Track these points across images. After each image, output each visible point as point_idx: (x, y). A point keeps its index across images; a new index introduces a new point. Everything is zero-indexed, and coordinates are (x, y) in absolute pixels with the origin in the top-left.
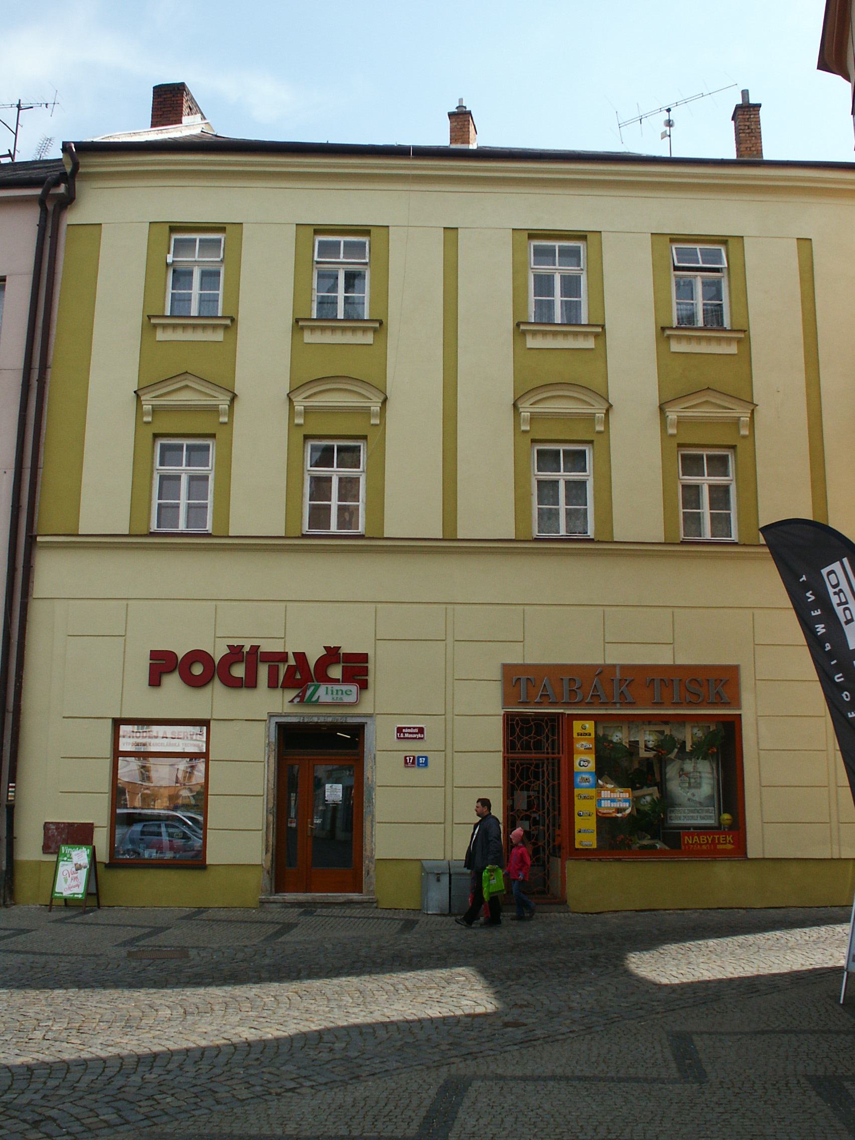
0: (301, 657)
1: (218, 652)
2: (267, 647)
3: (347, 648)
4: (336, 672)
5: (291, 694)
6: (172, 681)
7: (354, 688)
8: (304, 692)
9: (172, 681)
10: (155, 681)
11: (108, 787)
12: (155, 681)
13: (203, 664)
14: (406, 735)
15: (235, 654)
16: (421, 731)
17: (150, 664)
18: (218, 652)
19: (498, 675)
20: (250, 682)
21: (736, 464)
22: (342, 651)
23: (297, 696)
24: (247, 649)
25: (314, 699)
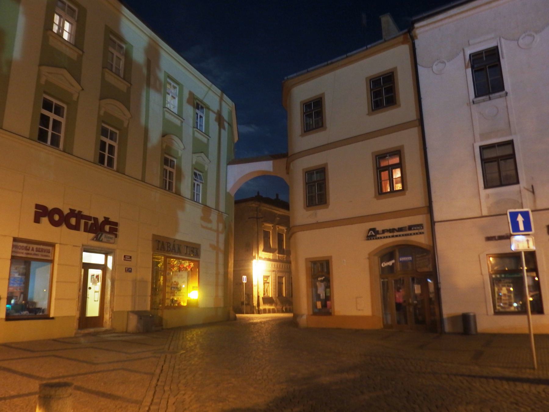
0: (96, 219)
1: (66, 211)
2: (86, 213)
3: (112, 219)
4: (107, 228)
5: (92, 235)
6: (45, 220)
7: (113, 236)
8: (97, 236)
9: (45, 220)
10: (37, 220)
11: (49, 283)
12: (37, 220)
13: (71, 218)
14: (127, 259)
15: (72, 213)
16: (131, 257)
17: (117, 232)
18: (66, 211)
19: (150, 238)
20: (76, 228)
21: (508, 221)
22: (109, 220)
23: (95, 237)
24: (76, 212)
25: (101, 239)
